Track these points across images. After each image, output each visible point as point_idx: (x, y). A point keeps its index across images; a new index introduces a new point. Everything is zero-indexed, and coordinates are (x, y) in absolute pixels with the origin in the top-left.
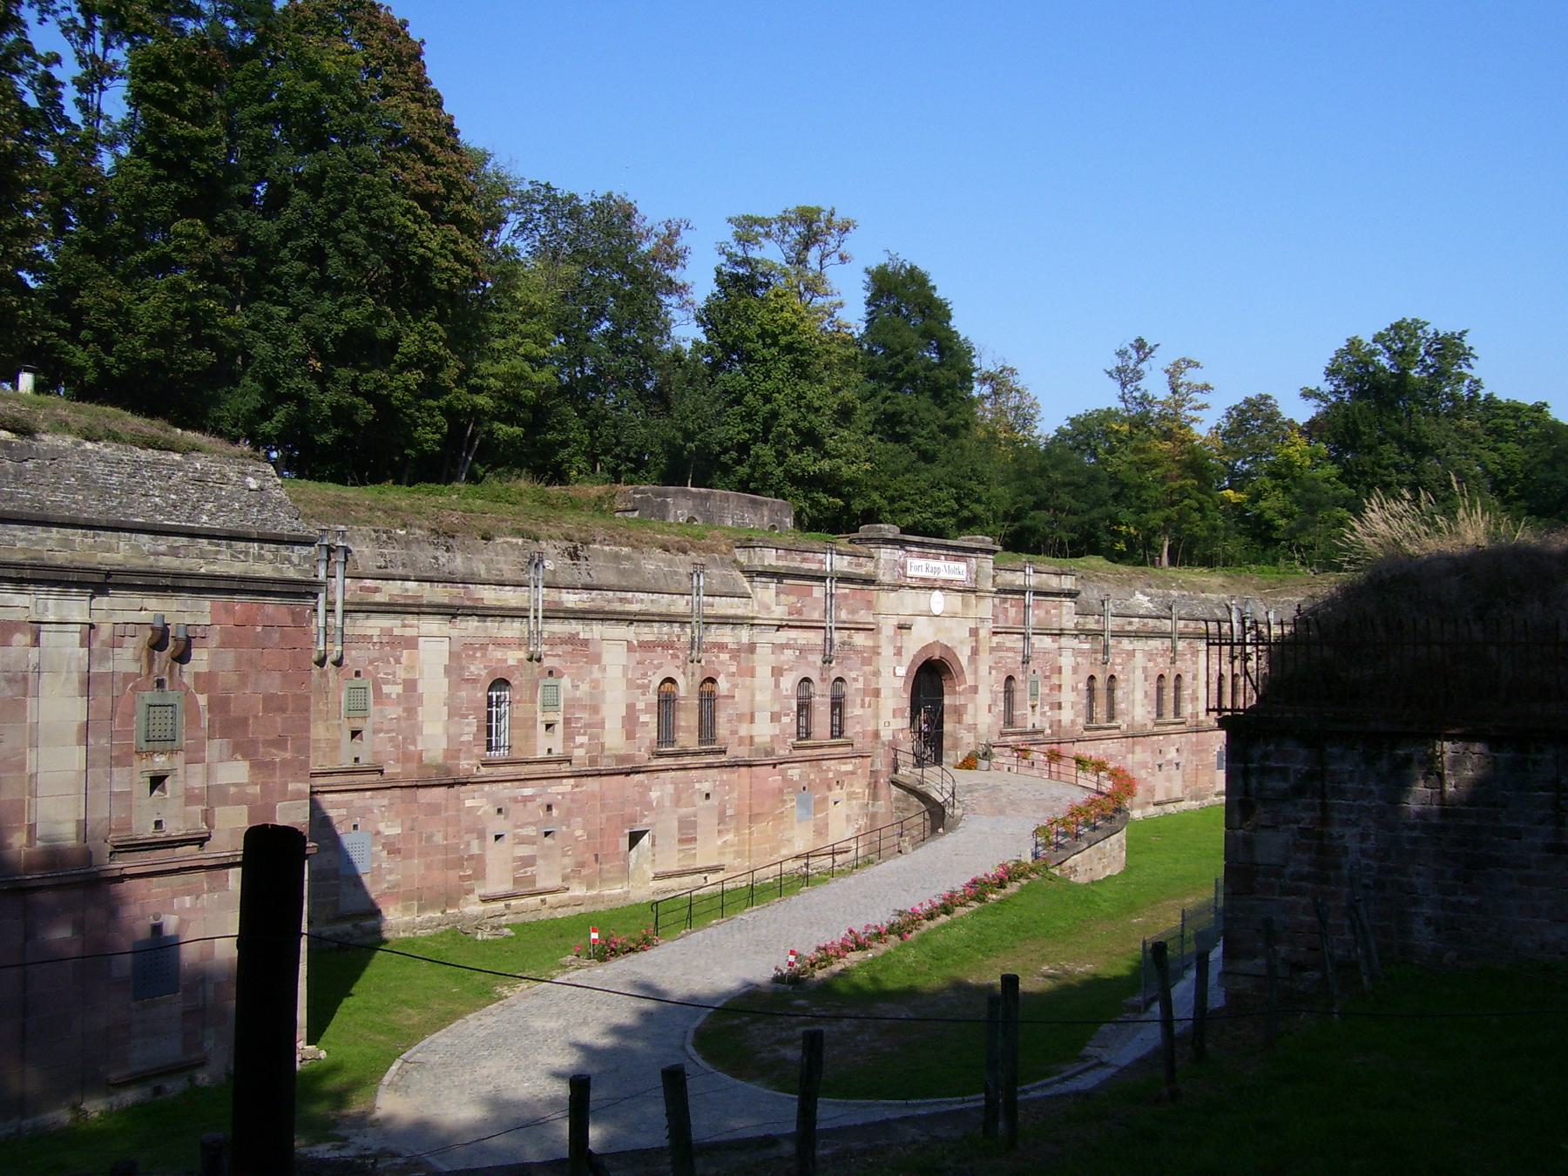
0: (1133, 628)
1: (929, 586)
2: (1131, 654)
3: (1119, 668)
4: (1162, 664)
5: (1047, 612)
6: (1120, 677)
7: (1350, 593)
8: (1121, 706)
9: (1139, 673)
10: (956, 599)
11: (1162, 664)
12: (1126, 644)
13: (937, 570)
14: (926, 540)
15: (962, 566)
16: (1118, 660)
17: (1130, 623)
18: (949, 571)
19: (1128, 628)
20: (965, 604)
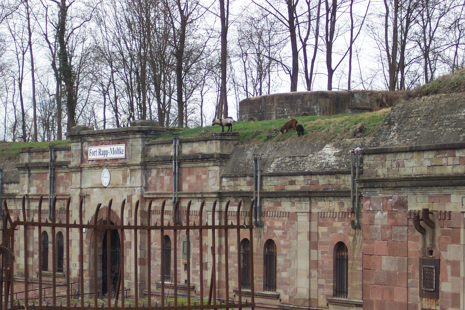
0: (297, 187)
1: (100, 165)
2: (293, 217)
3: (278, 233)
4: (341, 230)
5: (198, 177)
6: (280, 242)
7: (68, 116)
8: (282, 275)
9: (303, 238)
10: (119, 174)
11: (341, 230)
12: (286, 206)
13: (106, 153)
14: (65, 257)
15: (122, 147)
16: (278, 224)
17: (292, 183)
18: (114, 152)
19: (290, 188)
20: (90, 111)
